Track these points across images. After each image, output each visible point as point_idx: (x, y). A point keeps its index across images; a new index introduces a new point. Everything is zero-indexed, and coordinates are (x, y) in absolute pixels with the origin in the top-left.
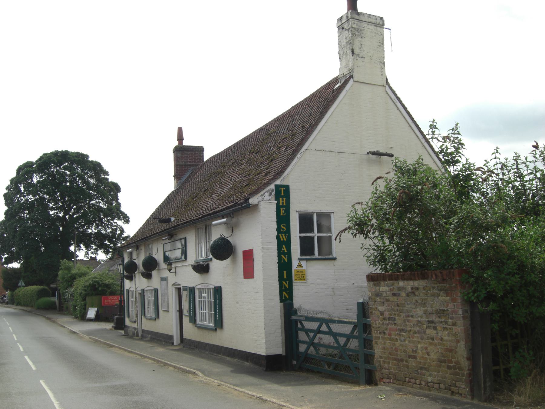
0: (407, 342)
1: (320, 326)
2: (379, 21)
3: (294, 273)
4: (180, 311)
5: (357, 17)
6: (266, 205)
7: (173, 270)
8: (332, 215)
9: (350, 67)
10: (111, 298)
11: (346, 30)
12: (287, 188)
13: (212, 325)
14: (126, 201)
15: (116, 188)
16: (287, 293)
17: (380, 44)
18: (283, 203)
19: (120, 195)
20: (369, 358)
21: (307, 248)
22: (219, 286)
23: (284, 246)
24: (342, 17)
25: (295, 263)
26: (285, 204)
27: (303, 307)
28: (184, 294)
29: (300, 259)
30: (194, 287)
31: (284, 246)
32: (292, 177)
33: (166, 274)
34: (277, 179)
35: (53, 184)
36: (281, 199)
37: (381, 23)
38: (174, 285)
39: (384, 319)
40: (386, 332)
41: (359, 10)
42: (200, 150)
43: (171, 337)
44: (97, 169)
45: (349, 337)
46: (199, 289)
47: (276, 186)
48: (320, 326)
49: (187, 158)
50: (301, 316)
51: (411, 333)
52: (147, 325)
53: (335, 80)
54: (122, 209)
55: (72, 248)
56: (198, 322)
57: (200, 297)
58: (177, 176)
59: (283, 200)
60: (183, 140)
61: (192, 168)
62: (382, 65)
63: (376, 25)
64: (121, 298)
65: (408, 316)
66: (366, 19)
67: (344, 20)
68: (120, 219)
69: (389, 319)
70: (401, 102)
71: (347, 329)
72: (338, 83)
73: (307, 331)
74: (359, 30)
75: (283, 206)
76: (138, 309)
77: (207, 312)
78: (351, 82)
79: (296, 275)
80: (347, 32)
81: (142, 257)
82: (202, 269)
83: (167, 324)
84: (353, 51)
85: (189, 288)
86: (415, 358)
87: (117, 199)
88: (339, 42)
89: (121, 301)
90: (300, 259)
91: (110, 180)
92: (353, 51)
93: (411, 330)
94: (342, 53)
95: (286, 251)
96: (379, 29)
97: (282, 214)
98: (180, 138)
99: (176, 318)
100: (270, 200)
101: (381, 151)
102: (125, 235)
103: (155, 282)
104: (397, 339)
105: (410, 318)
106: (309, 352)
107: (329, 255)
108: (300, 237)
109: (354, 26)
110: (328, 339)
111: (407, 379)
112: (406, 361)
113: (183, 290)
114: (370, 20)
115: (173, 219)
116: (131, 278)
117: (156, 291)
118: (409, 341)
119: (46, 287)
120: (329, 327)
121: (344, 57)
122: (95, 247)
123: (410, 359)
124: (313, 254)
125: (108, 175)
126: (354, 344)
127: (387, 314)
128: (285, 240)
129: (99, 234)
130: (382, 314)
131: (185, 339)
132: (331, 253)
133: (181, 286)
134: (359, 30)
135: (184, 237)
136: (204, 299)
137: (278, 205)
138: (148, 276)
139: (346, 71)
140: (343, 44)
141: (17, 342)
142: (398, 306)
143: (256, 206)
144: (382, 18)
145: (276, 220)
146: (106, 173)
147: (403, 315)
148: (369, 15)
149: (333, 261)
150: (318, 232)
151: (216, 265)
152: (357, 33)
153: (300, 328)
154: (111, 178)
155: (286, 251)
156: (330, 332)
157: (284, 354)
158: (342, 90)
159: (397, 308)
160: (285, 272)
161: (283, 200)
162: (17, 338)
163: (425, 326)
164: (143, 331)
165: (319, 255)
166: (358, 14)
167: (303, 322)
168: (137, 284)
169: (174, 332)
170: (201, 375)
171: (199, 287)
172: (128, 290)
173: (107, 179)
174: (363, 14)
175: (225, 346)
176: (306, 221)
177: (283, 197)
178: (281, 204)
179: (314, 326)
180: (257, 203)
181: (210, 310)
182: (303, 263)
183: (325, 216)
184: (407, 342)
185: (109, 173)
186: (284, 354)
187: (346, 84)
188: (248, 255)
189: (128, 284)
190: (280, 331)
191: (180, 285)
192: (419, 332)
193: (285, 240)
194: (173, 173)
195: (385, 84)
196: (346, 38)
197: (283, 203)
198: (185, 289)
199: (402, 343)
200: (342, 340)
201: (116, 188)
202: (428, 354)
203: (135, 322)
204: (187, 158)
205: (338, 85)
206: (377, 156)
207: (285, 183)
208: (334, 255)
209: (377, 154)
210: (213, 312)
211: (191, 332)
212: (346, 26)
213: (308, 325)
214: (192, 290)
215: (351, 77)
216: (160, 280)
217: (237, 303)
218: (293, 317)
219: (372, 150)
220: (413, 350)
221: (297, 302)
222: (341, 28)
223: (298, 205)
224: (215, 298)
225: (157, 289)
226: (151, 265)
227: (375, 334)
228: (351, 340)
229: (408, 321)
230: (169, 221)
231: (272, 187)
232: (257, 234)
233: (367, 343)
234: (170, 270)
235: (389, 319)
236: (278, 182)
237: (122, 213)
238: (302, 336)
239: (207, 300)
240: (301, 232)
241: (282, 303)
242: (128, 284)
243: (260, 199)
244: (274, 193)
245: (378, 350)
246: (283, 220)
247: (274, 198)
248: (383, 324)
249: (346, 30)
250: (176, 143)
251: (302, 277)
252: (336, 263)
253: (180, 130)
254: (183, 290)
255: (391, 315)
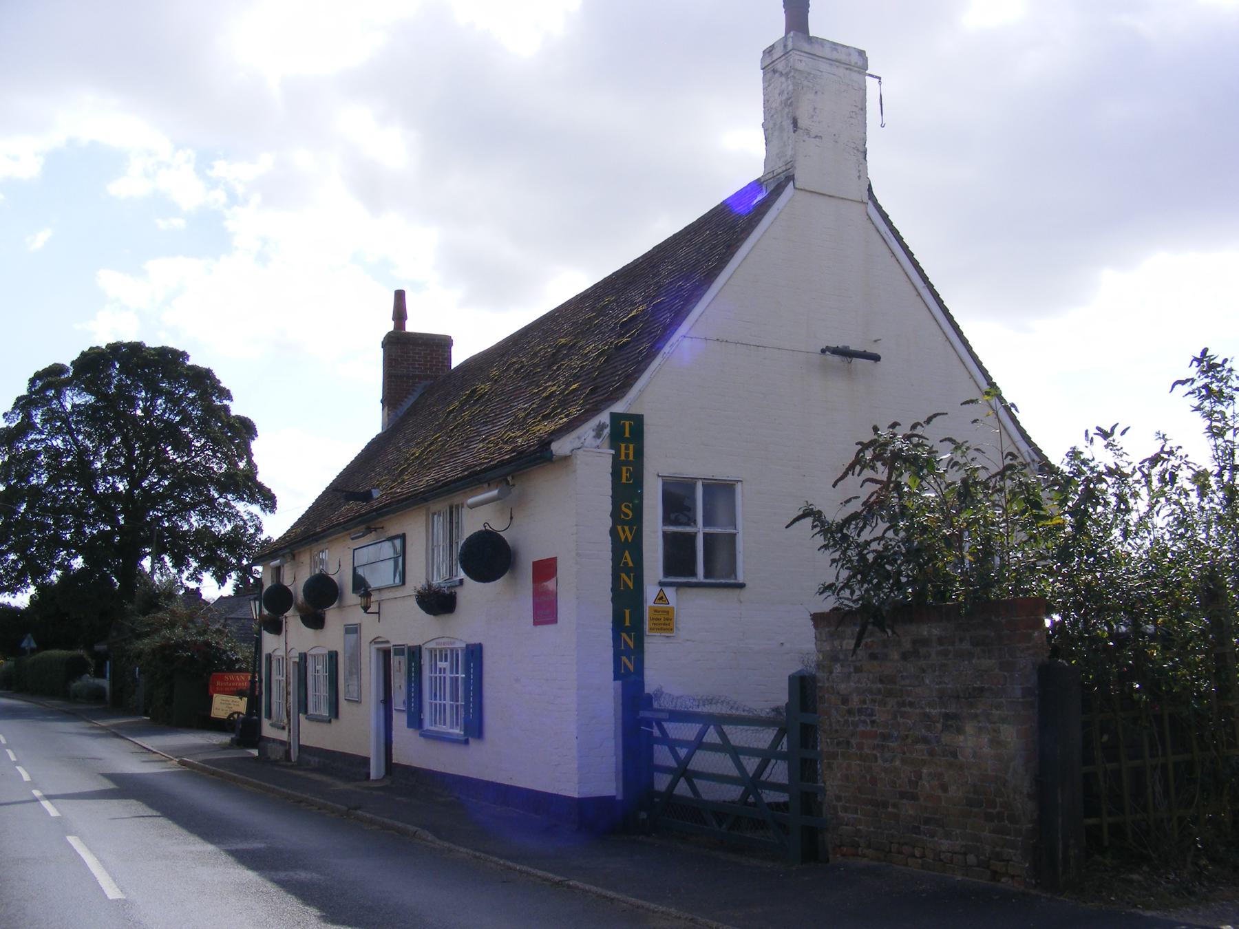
0: (897, 763)
1: (702, 733)
2: (855, 58)
3: (647, 615)
4: (387, 701)
5: (807, 47)
6: (587, 454)
7: (373, 608)
8: (739, 487)
9: (788, 158)
10: (232, 678)
11: (781, 74)
12: (637, 422)
13: (458, 731)
14: (270, 459)
15: (246, 429)
16: (630, 660)
17: (856, 109)
18: (627, 455)
19: (255, 446)
20: (809, 801)
21: (679, 559)
22: (477, 642)
23: (627, 554)
24: (773, 47)
25: (651, 592)
26: (631, 458)
27: (665, 690)
28: (399, 665)
29: (662, 584)
30: (420, 647)
31: (627, 554)
32: (648, 396)
33: (356, 616)
34: (617, 399)
35: (108, 415)
36: (623, 445)
37: (860, 63)
38: (374, 641)
39: (850, 712)
40: (853, 741)
41: (813, 32)
42: (442, 345)
43: (365, 761)
44: (204, 381)
45: (766, 756)
46: (431, 651)
47: (614, 416)
48: (702, 733)
49: (412, 362)
50: (662, 711)
51: (909, 741)
52: (313, 735)
53: (756, 185)
54: (259, 478)
55: (146, 563)
56: (427, 725)
57: (434, 668)
58: (390, 400)
59: (627, 448)
60: (406, 318)
61: (424, 383)
62: (861, 156)
63: (848, 66)
64: (254, 677)
65: (903, 704)
66: (827, 52)
67: (778, 52)
68: (252, 500)
69: (860, 711)
70: (899, 239)
71: (763, 738)
72: (760, 192)
73: (672, 744)
74: (810, 81)
75: (626, 463)
76: (291, 698)
77: (448, 702)
78: (790, 188)
79: (651, 619)
80: (783, 79)
81: (305, 575)
82: (438, 602)
83: (355, 731)
84: (795, 123)
85: (409, 648)
86: (914, 797)
87: (249, 455)
88: (766, 102)
89: (253, 682)
90: (662, 584)
91: (233, 413)
92: (795, 123)
93: (907, 736)
94: (771, 125)
95: (631, 564)
96: (855, 76)
97: (624, 480)
98: (400, 314)
99: (377, 686)
100: (598, 447)
101: (853, 348)
102: (263, 537)
103: (332, 637)
104: (876, 757)
105: (908, 709)
106: (676, 792)
107: (728, 577)
108: (665, 534)
109: (800, 66)
110: (721, 764)
111: (895, 847)
112: (895, 806)
113: (395, 654)
114: (835, 55)
115: (376, 494)
116: (276, 627)
117: (333, 656)
118: (903, 761)
119: (80, 652)
120: (722, 735)
121: (776, 133)
122: (195, 564)
123: (904, 801)
124: (694, 574)
125: (230, 398)
126: (779, 772)
127: (855, 701)
128: (630, 539)
129: (204, 534)
130: (845, 701)
131: (397, 765)
132: (733, 571)
133: (390, 645)
134: (810, 81)
135: (400, 532)
136: (441, 676)
137: (615, 458)
138: (315, 620)
139: (779, 167)
140: (774, 106)
141: (16, 763)
142: (881, 681)
143: (566, 459)
144: (862, 53)
145: (610, 493)
146: (226, 394)
147: (892, 702)
148: (834, 44)
149: (737, 591)
150: (705, 524)
151: (472, 593)
152: (805, 83)
153: (657, 738)
154: (237, 408)
155: (631, 564)
156: (725, 747)
157: (620, 797)
158: (769, 207)
159: (880, 686)
160: (627, 612)
161: (627, 448)
162: (16, 755)
163: (939, 726)
164: (302, 748)
165: (706, 576)
166: (811, 40)
167: (665, 725)
168: (294, 640)
169: (369, 748)
170: (430, 837)
171: (432, 645)
172: (269, 657)
173: (226, 408)
174: (821, 42)
175: (486, 779)
176: (677, 501)
177: (627, 441)
178: (623, 457)
179: (687, 731)
180: (568, 453)
181: (455, 697)
182: (670, 593)
183: (720, 491)
184: (897, 763)
185: (233, 393)
186: (620, 797)
187: (779, 195)
188: (545, 570)
189: (270, 643)
190: (611, 743)
191: (388, 642)
192: (925, 740)
193: (630, 539)
194: (379, 395)
195: (866, 198)
196: (781, 93)
197: (627, 455)
198: (400, 650)
199: (887, 765)
200: (751, 764)
201: (246, 429)
202: (944, 788)
203: (284, 728)
204: (412, 362)
205: (759, 198)
206: (844, 358)
207: (634, 411)
208: (741, 578)
209: (845, 353)
210: (461, 702)
211: (410, 749)
212: (780, 66)
213: (677, 731)
214: (414, 654)
215: (790, 178)
216: (342, 632)
217: (517, 680)
218: (644, 714)
219: (833, 345)
220: (910, 781)
221: (654, 679)
222: (769, 69)
223: (663, 460)
224: (467, 671)
225: (336, 653)
226: (323, 592)
227: (824, 744)
228: (773, 761)
229: (903, 715)
230: (367, 496)
231: (604, 417)
232: (567, 517)
233: (806, 768)
234: (366, 608)
235: (860, 711)
236: (619, 407)
237: (261, 487)
238: (662, 756)
239: (448, 675)
240: (667, 520)
241: (619, 682)
242: (270, 643)
243: (577, 444)
244: (607, 431)
245: (832, 782)
246: (626, 491)
247: (607, 443)
248: (846, 721)
249: (781, 74)
250: (390, 326)
251: (666, 622)
252: (744, 594)
253: (400, 296)
254: (395, 654)
255: (864, 702)
